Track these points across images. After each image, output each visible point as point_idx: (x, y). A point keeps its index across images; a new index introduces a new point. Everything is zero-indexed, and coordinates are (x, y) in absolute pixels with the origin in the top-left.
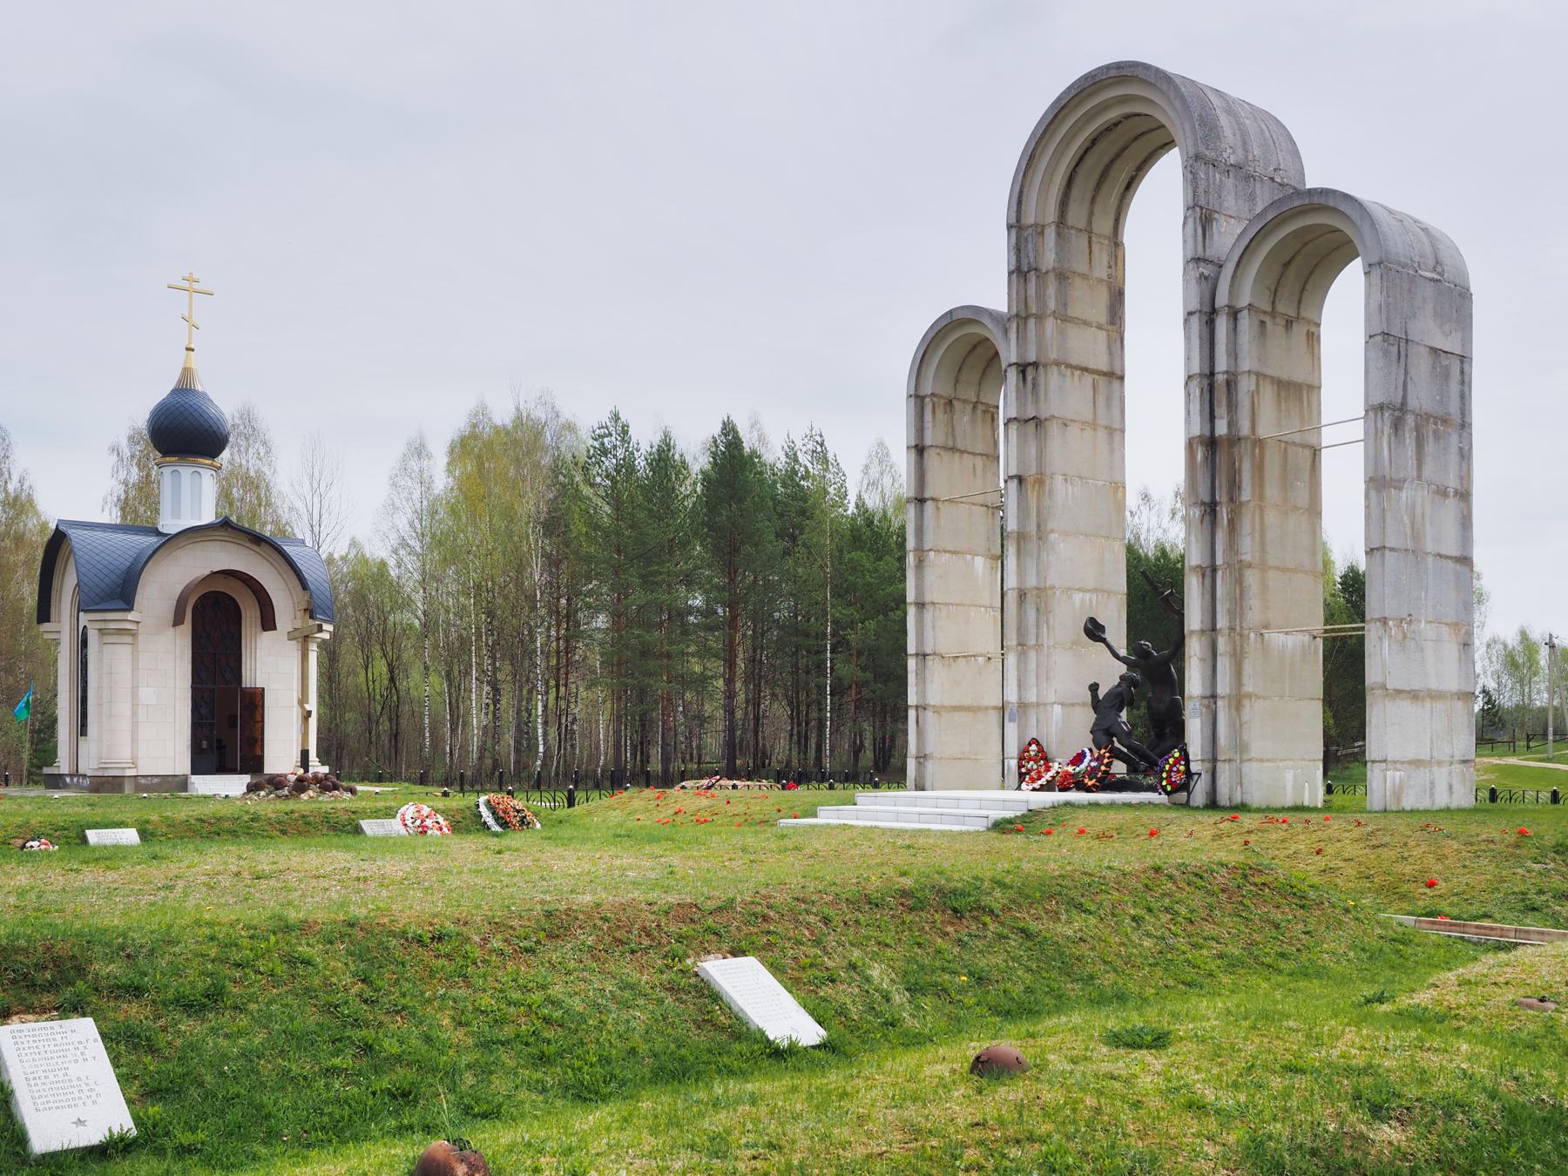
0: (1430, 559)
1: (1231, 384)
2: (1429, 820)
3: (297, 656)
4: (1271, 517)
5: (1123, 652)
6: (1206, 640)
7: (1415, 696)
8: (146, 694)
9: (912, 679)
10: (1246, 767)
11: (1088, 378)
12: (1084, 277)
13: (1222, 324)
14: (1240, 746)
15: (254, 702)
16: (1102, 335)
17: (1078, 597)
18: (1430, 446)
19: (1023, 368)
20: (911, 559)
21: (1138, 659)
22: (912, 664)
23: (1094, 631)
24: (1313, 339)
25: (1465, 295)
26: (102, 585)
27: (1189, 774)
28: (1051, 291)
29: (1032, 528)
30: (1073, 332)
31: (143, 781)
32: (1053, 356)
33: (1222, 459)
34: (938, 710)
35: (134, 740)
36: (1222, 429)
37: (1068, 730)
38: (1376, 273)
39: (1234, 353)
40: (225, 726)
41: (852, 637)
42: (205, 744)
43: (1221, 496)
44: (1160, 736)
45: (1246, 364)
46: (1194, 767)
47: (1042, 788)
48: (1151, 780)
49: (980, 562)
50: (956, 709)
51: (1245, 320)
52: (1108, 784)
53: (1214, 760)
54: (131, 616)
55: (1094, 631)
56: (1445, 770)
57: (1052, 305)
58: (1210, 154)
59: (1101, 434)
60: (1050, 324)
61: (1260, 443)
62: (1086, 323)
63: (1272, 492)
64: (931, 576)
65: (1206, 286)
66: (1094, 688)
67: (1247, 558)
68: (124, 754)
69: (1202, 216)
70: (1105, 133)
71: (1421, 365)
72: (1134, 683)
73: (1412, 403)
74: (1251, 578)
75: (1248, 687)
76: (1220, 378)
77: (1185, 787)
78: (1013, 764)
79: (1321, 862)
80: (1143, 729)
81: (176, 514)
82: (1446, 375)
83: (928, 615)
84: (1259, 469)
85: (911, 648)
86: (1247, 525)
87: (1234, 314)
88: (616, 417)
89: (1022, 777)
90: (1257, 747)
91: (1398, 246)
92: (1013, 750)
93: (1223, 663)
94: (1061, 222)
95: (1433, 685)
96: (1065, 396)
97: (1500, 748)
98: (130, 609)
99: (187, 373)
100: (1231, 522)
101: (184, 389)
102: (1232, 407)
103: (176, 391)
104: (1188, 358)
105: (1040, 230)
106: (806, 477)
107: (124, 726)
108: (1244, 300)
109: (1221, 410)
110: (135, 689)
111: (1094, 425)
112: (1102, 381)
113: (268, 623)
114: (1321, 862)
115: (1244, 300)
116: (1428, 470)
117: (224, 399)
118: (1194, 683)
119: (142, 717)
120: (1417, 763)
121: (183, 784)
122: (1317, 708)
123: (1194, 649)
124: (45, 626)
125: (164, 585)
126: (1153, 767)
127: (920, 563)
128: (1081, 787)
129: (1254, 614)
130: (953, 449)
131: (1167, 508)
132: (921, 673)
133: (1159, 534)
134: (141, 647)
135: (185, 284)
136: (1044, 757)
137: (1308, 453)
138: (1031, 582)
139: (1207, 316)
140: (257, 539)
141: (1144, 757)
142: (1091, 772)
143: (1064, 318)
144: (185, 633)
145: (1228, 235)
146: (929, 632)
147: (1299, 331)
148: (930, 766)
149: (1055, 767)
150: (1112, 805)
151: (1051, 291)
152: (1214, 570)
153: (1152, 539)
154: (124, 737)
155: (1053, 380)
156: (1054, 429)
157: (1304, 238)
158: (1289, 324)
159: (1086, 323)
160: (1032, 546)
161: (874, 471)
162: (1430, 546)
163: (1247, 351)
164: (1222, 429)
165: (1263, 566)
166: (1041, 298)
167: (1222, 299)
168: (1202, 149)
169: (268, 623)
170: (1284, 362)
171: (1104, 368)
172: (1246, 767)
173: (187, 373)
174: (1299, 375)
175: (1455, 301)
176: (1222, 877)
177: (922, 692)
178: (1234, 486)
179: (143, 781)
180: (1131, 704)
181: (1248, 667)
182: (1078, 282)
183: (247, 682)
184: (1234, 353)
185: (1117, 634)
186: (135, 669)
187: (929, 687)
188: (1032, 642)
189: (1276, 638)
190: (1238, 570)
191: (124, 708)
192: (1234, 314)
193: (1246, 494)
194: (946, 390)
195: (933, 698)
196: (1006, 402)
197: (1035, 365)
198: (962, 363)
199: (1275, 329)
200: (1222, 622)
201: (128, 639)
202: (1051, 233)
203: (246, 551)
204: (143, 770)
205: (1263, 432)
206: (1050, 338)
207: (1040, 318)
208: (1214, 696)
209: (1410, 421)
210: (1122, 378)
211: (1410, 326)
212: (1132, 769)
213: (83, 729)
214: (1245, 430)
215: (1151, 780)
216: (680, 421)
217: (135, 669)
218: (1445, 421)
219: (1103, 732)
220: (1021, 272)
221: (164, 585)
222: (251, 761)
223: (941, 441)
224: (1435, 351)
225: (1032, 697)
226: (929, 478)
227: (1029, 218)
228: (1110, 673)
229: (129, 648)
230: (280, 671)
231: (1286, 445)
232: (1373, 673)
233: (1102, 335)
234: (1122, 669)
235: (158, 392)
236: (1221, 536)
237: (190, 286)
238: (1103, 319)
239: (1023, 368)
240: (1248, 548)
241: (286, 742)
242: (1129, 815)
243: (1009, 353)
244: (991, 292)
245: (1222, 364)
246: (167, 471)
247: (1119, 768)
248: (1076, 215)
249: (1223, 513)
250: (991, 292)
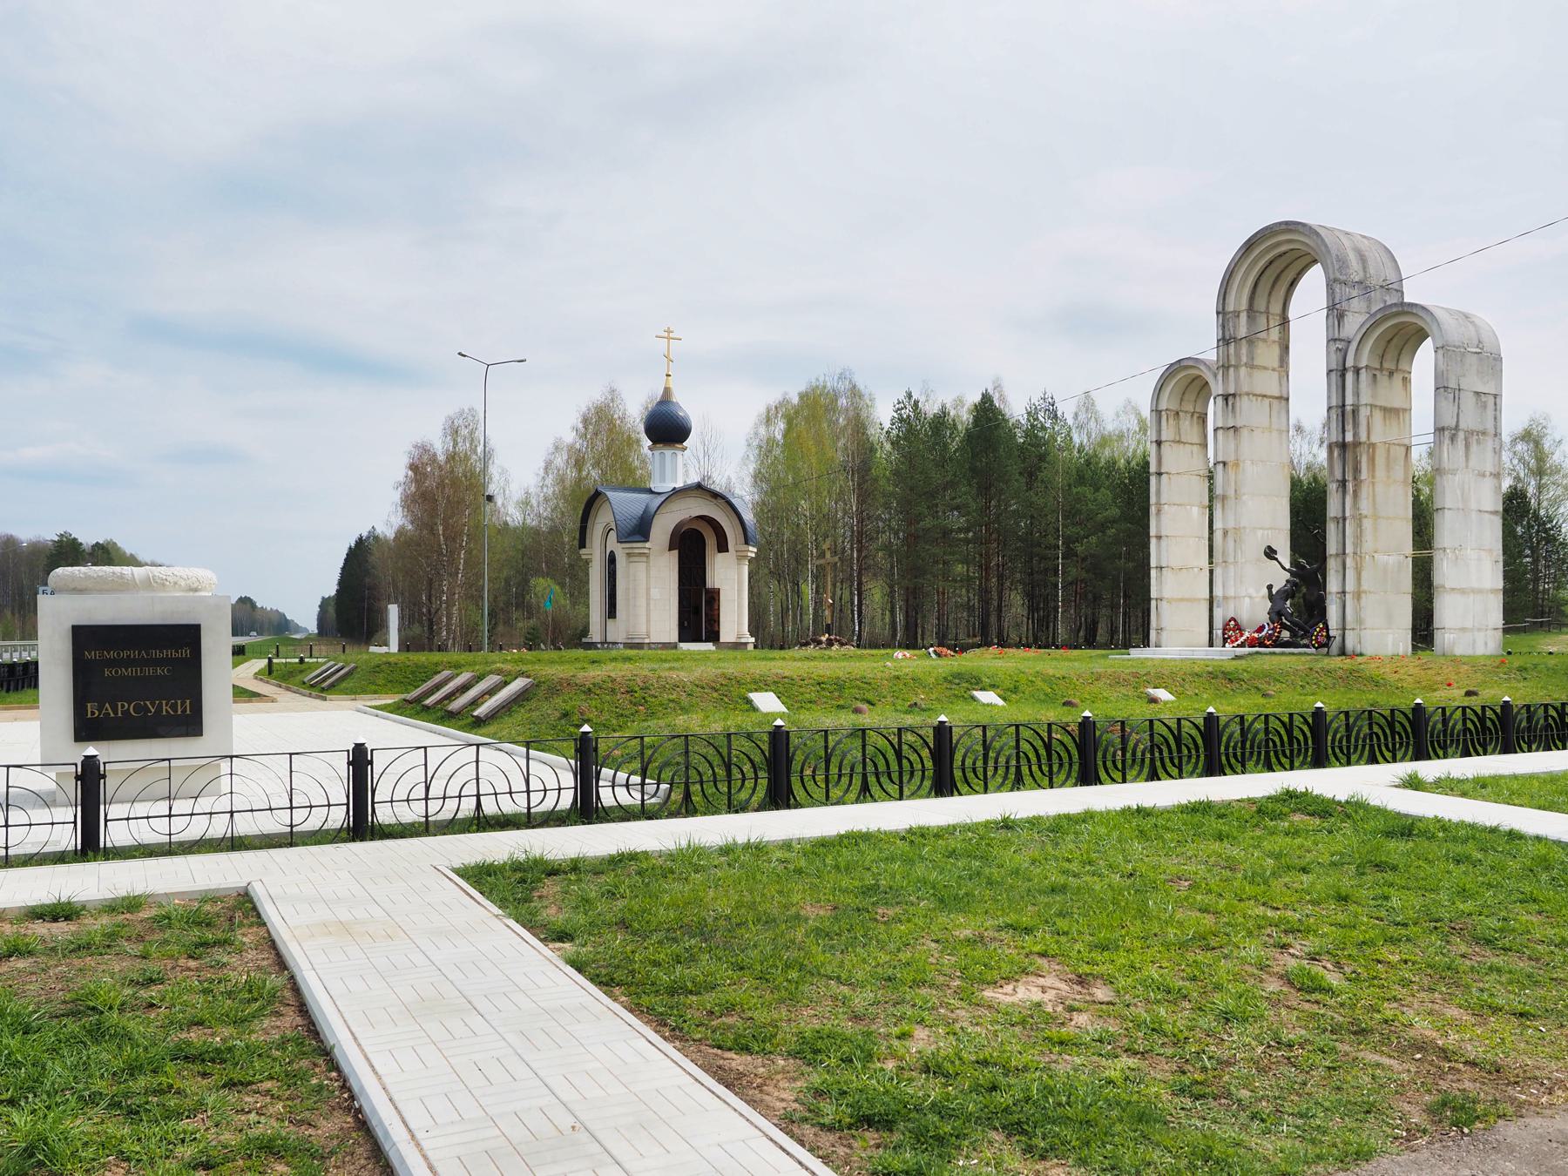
0: (1474, 515)
1: (1355, 412)
2: (1472, 662)
4: (1379, 488)
5: (1288, 566)
6: (1339, 560)
7: (1463, 591)
8: (655, 593)
9: (1153, 581)
10: (1363, 633)
11: (1267, 401)
12: (1264, 340)
13: (1350, 377)
14: (1360, 621)
15: (714, 596)
16: (1276, 374)
17: (1260, 533)
18: (1474, 448)
19: (1226, 397)
20: (1153, 510)
21: (1297, 571)
22: (1153, 573)
23: (1270, 553)
24: (1406, 381)
25: (1498, 359)
27: (1328, 637)
28: (1244, 351)
29: (1231, 493)
30: (1258, 374)
32: (1245, 389)
33: (1349, 455)
34: (1170, 601)
35: (648, 621)
36: (1349, 438)
37: (1253, 608)
38: (1440, 352)
39: (1357, 394)
40: (698, 614)
41: (1079, 548)
43: (1349, 477)
44: (1311, 616)
45: (1364, 399)
46: (1332, 633)
47: (1242, 645)
48: (1305, 641)
49: (1195, 510)
50: (1182, 600)
51: (1363, 373)
52: (1278, 643)
53: (1344, 629)
54: (647, 545)
55: (1270, 553)
56: (1482, 634)
57: (1244, 359)
58: (1343, 278)
59: (1275, 434)
60: (1243, 370)
61: (1373, 446)
62: (1265, 368)
63: (1380, 472)
64: (1164, 517)
65: (1340, 355)
66: (1270, 587)
67: (1364, 512)
68: (643, 630)
69: (1336, 313)
70: (1273, 262)
71: (1468, 401)
72: (1295, 584)
73: (1462, 425)
74: (1367, 524)
75: (1365, 586)
76: (1349, 408)
77: (1326, 645)
78: (1218, 632)
79: (1397, 676)
80: (1303, 610)
81: (663, 479)
82: (1485, 406)
83: (1164, 542)
84: (1372, 460)
85: (1153, 563)
86: (1365, 491)
87: (1357, 371)
88: (910, 396)
89: (1225, 640)
90: (1369, 622)
91: (1453, 331)
92: (1218, 624)
93: (1350, 573)
94: (1251, 308)
95: (1475, 585)
96: (1251, 412)
99: (667, 391)
100: (1355, 492)
102: (1356, 425)
103: (661, 403)
104: (1329, 397)
105: (1237, 314)
106: (1043, 428)
107: (642, 611)
108: (1363, 363)
109: (1349, 427)
110: (648, 590)
111: (1270, 429)
112: (1275, 402)
113: (723, 547)
114: (1397, 676)
115: (1363, 363)
116: (1472, 463)
117: (688, 405)
118: (1333, 585)
120: (1463, 630)
121: (674, 646)
123: (1332, 565)
124: (583, 551)
125: (662, 529)
126: (1307, 634)
127: (1159, 511)
128: (1262, 645)
129: (1368, 544)
130: (1179, 442)
131: (1317, 437)
132: (1159, 578)
133: (1310, 458)
136: (1239, 628)
137: (1403, 449)
138: (1231, 524)
139: (1339, 373)
140: (715, 495)
141: (1301, 628)
142: (1269, 637)
143: (1251, 366)
144: (676, 553)
145: (1353, 324)
146: (1164, 553)
147: (1398, 378)
148: (1164, 635)
149: (1247, 634)
150: (1283, 654)
151: (1244, 351)
152: (1344, 519)
153: (1303, 463)
154: (643, 619)
155: (1244, 404)
156: (1245, 433)
157: (1400, 328)
158: (1391, 374)
159: (1265, 368)
160: (1230, 503)
161: (1082, 417)
162: (1474, 506)
163: (1365, 393)
164: (1349, 438)
165: (1376, 517)
166: (1238, 355)
167: (1350, 363)
168: (1338, 275)
169: (723, 547)
170: (1389, 393)
171: (1277, 394)
172: (1363, 633)
173: (667, 391)
174: (1397, 403)
175: (1491, 362)
176: (1340, 673)
177: (1160, 590)
178: (1357, 470)
180: (1293, 597)
181: (1364, 574)
182: (1261, 344)
183: (709, 585)
184: (1357, 394)
185: (1285, 557)
186: (648, 577)
187: (1162, 586)
188: (1231, 559)
189: (1381, 558)
190: (1359, 519)
191: (642, 602)
192: (1357, 371)
193: (1364, 475)
194: (1174, 406)
195: (1166, 595)
196: (1213, 409)
197: (1234, 395)
198: (1185, 385)
199: (1383, 379)
200: (1349, 550)
202: (1244, 316)
205: (1374, 439)
206: (1244, 380)
207: (1236, 367)
208: (1344, 592)
209: (1461, 435)
210: (1287, 399)
211: (1462, 380)
212: (1294, 634)
213: (611, 611)
214: (1363, 438)
215: (1305, 641)
216: (953, 396)
217: (648, 577)
218: (1484, 433)
219: (1276, 614)
220: (1225, 341)
221: (662, 529)
222: (714, 636)
223: (1171, 437)
224: (1477, 393)
225: (1231, 593)
226: (1164, 460)
227: (1230, 307)
228: (1280, 579)
230: (730, 577)
231: (1388, 445)
232: (1438, 579)
233: (1276, 374)
234: (1288, 576)
236: (1349, 499)
238: (1276, 364)
239: (1226, 397)
240: (1365, 506)
241: (734, 620)
242: (1294, 658)
243: (1217, 388)
244: (1203, 344)
245: (1349, 400)
246: (657, 453)
247: (1286, 635)
248: (1260, 304)
249: (1350, 486)
250: (1203, 344)
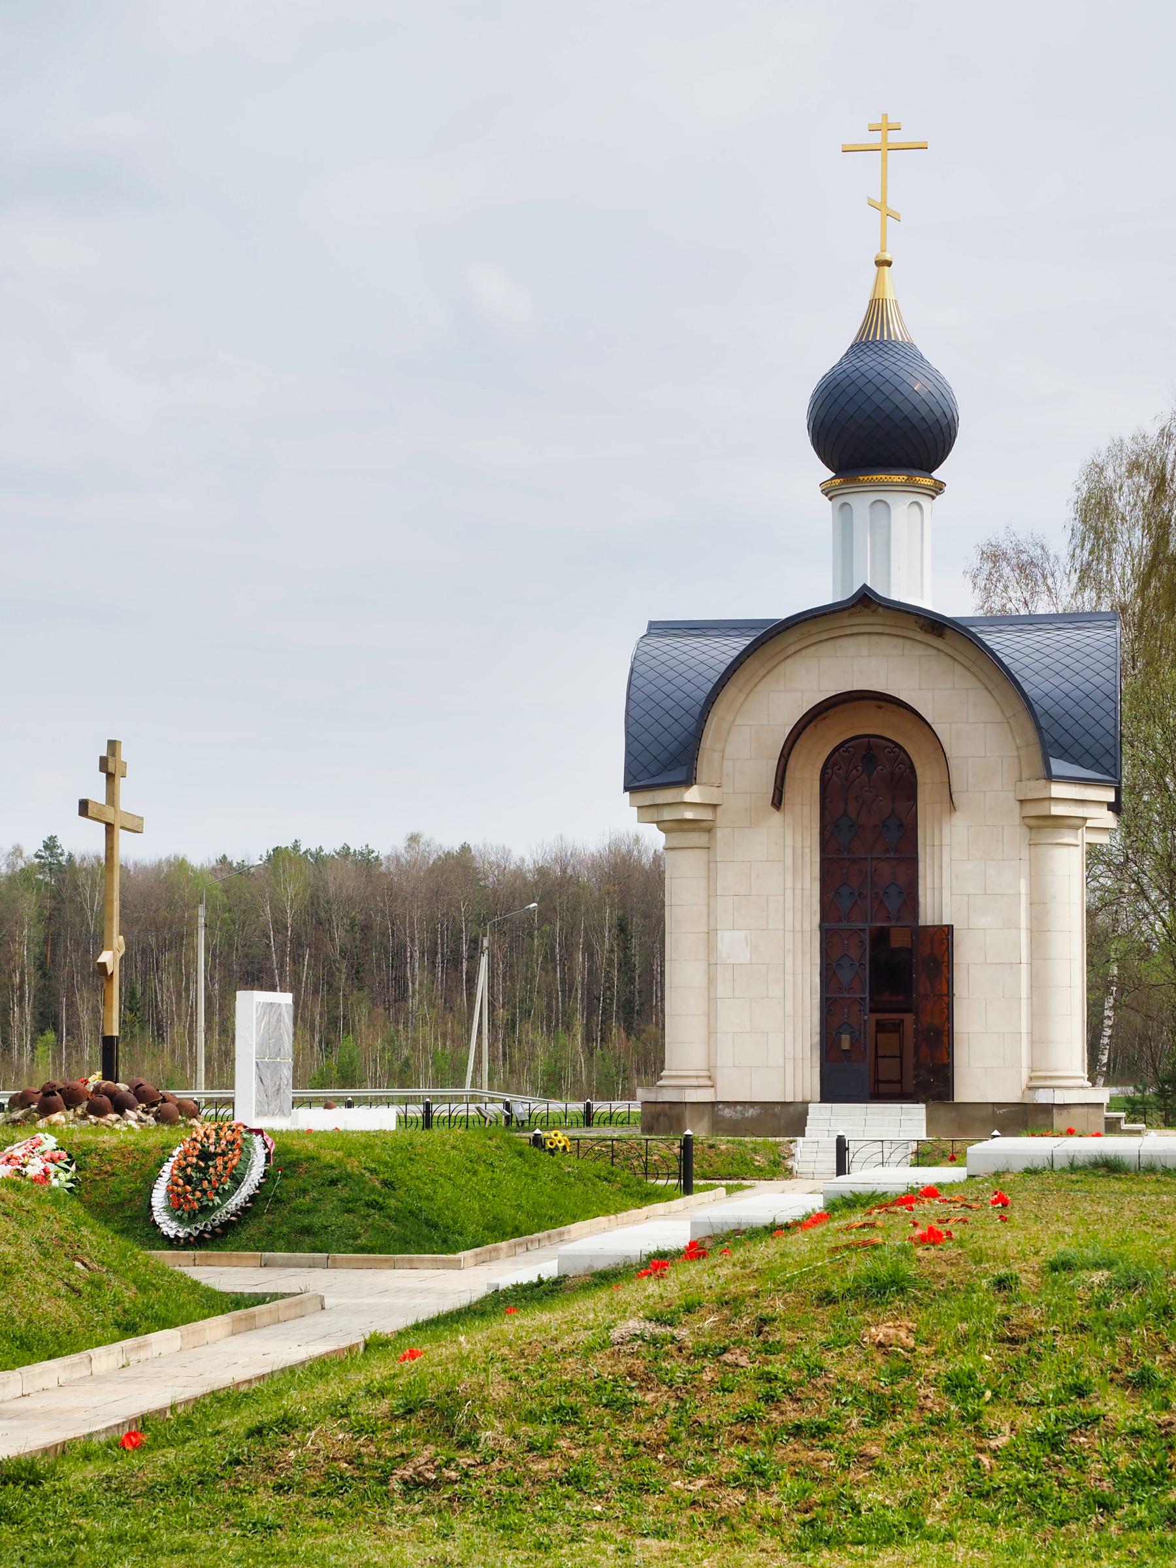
3: (1065, 850)
8: (733, 944)
26: (666, 738)
31: (727, 1112)
42: (846, 1042)
54: (692, 794)
97: (1018, 1166)
98: (689, 781)
99: (877, 309)
101: (873, 339)
103: (861, 346)
110: (711, 934)
119: (722, 989)
122: (255, 992)
134: (721, 851)
135: (876, 138)
173: (877, 309)
179: (727, 1112)
183: (928, 916)
186: (711, 895)
201: (698, 839)
203: (919, 650)
204: (726, 1092)
217: (711, 895)
229: (701, 855)
235: (825, 350)
237: (885, 141)
